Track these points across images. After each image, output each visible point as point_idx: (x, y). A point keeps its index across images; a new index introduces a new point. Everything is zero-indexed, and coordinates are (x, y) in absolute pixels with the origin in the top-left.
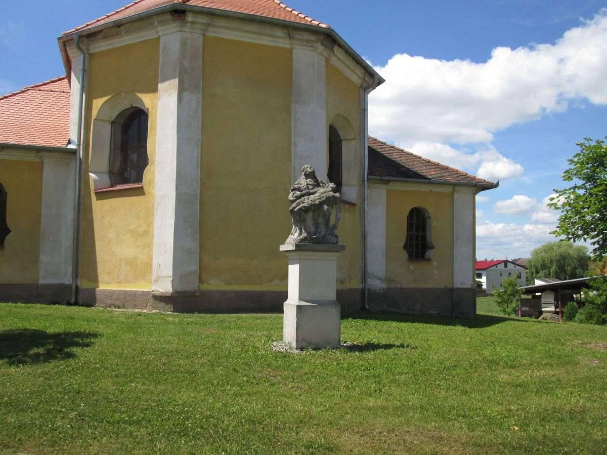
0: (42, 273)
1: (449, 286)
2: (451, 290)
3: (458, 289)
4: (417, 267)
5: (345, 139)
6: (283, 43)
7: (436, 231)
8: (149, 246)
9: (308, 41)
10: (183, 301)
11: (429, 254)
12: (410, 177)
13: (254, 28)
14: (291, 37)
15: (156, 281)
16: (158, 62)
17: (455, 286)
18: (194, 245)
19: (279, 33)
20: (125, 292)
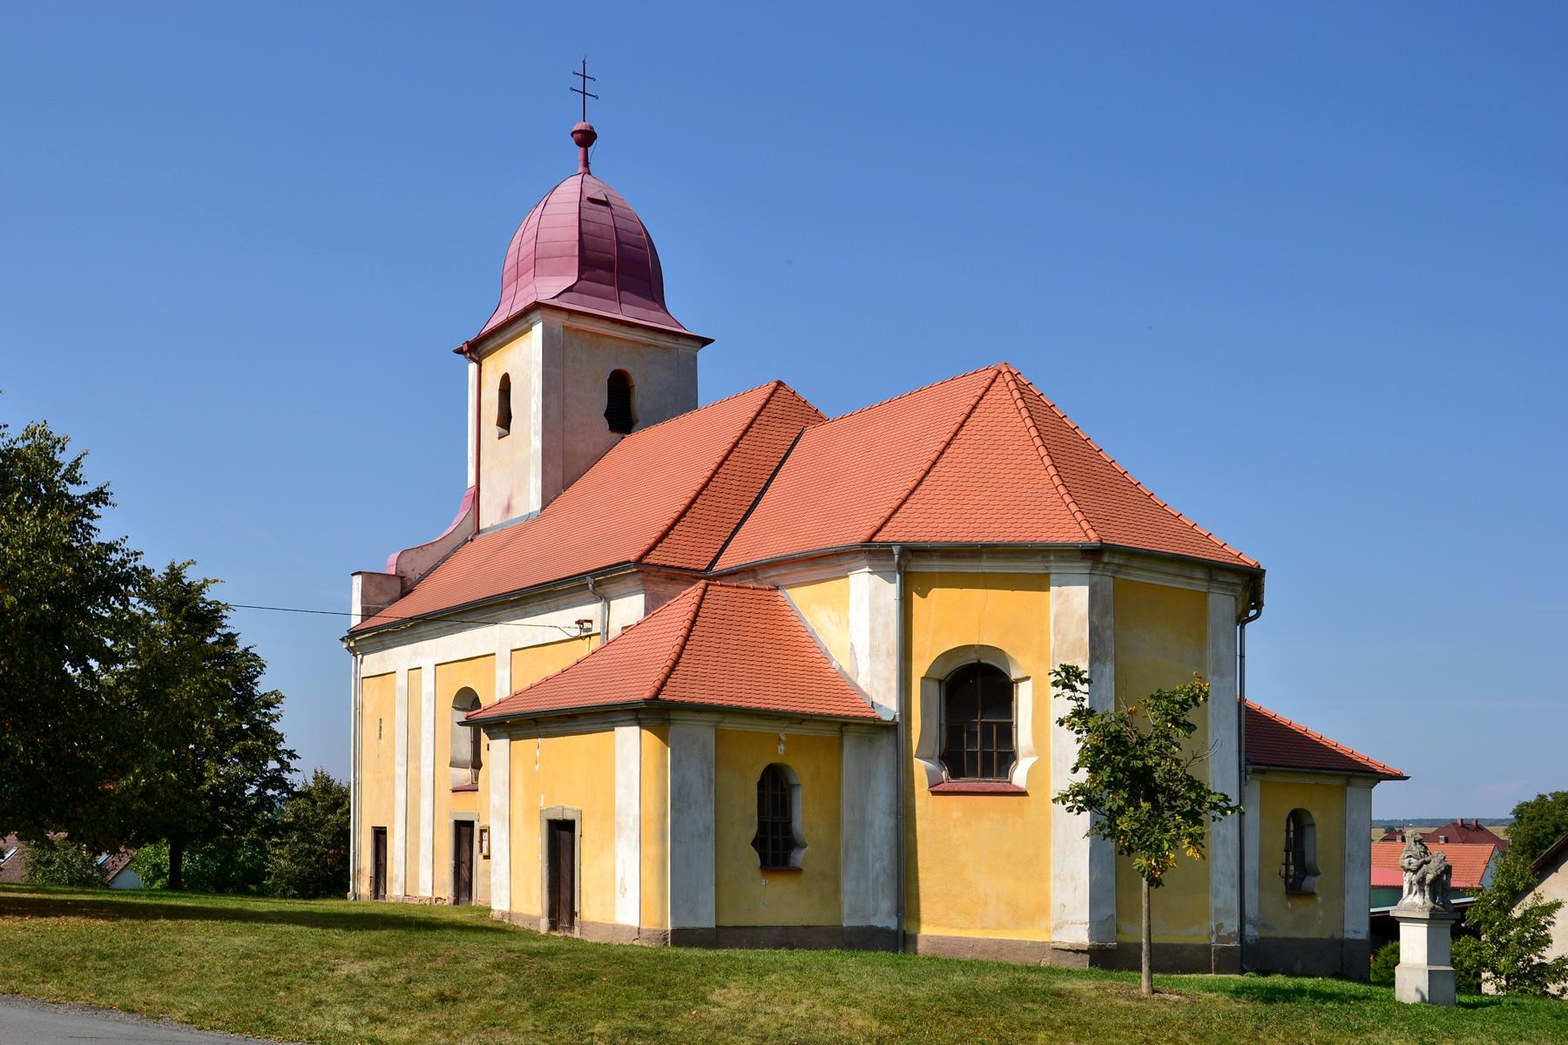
0: (846, 910)
1: (1338, 936)
2: (1342, 943)
3: (1349, 940)
4: (1302, 905)
5: (185, 565)
6: (1199, 586)
7: (805, 816)
8: (1042, 876)
9: (1229, 584)
10: (1107, 956)
11: (799, 857)
12: (1316, 770)
13: (1172, 569)
14: (1211, 579)
15: (1059, 927)
16: (1047, 615)
17: (1346, 936)
18: (1111, 879)
19: (1199, 574)
20: (1000, 942)
